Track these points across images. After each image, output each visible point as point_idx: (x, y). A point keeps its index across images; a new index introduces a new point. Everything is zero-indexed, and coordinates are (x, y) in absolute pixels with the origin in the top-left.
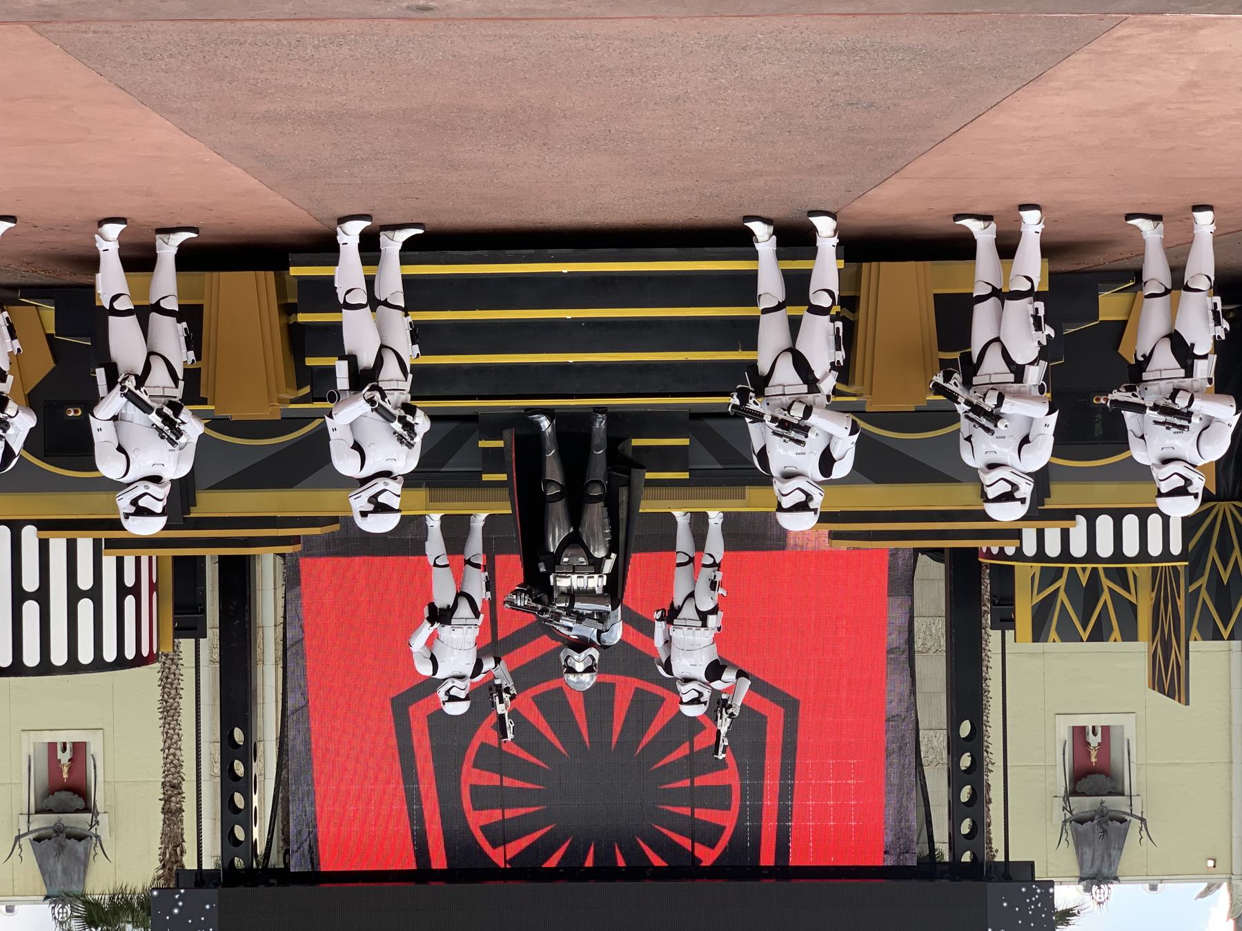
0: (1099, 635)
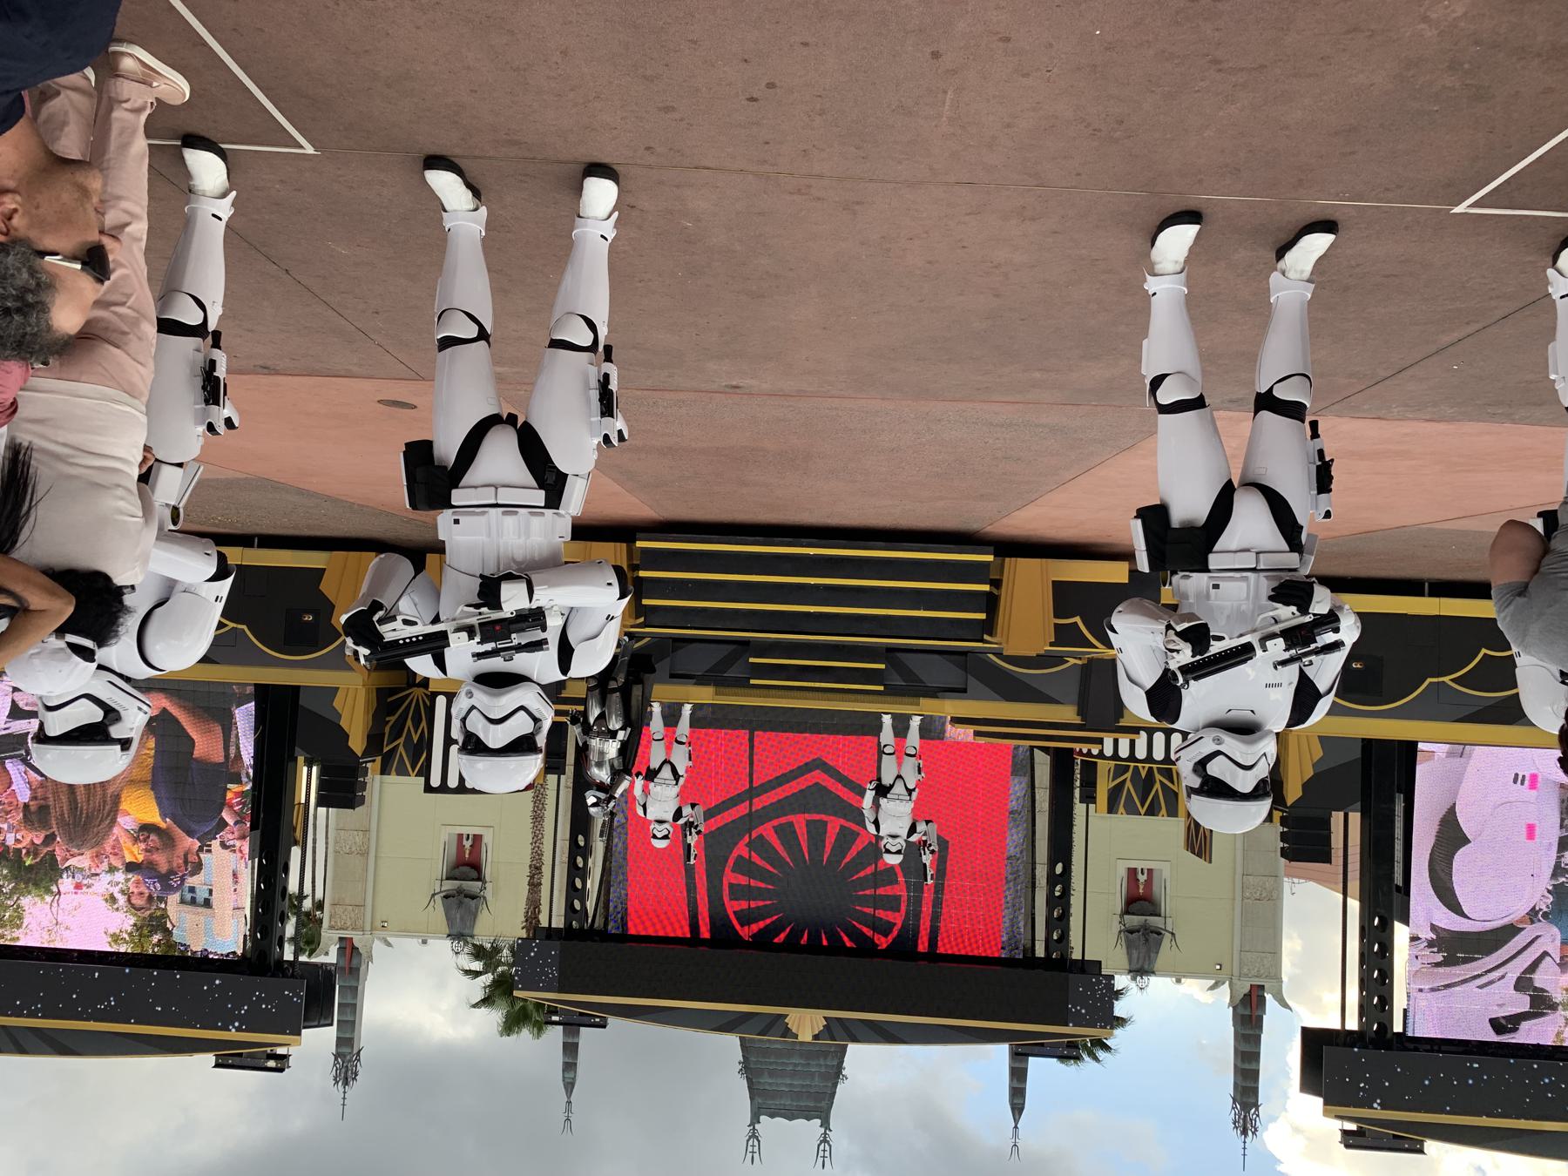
0: (1152, 811)
